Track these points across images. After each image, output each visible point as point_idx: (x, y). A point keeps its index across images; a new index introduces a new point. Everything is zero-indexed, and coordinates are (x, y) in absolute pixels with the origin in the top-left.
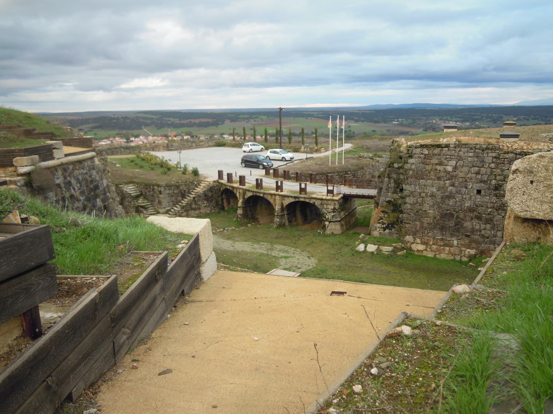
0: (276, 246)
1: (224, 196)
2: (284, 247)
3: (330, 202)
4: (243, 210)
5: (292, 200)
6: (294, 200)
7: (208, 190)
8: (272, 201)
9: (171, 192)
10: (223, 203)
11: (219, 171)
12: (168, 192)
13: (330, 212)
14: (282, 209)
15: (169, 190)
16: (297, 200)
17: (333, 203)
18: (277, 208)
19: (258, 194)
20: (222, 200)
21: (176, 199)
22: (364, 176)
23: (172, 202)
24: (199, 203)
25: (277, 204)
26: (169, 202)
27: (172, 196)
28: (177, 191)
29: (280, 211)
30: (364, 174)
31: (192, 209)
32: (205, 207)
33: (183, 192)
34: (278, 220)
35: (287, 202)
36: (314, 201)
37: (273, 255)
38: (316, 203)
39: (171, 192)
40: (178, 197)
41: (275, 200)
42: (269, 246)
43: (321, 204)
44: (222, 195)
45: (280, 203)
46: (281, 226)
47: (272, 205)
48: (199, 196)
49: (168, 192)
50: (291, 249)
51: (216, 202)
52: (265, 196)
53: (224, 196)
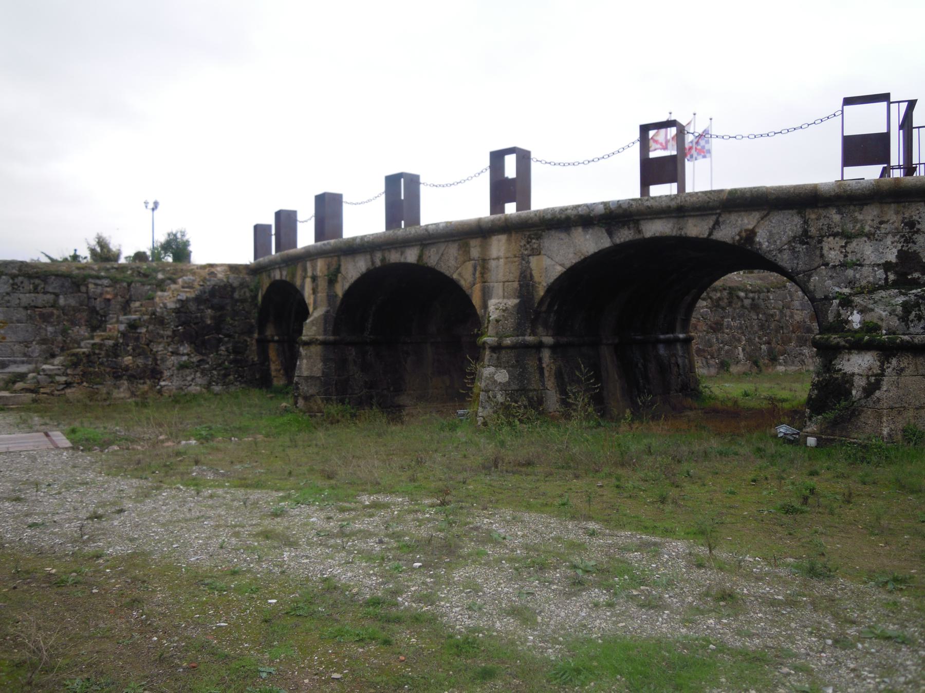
0: (492, 522)
1: (270, 331)
2: (573, 531)
3: (868, 216)
4: (325, 360)
5: (590, 243)
6: (605, 242)
7: (198, 300)
8: (464, 276)
10: (265, 358)
11: (257, 228)
12: (26, 299)
13: (874, 288)
14: (529, 310)
15: (36, 290)
16: (625, 235)
17: (893, 216)
18: (498, 305)
19: (394, 257)
20: (263, 343)
21: (64, 332)
22: (788, 312)
23: (44, 341)
24: (159, 348)
25: (498, 289)
27: (46, 318)
28: (72, 302)
29: (510, 323)
30: (787, 306)
31: (118, 374)
32: (183, 367)
33: (98, 304)
34: (502, 376)
35: (556, 259)
36: (748, 221)
37: (456, 614)
38: (762, 238)
40: (73, 323)
41: (483, 265)
42: (423, 521)
43: (804, 237)
44: (262, 327)
45: (514, 272)
46: (524, 403)
47: (466, 299)
48: (160, 321)
50: (653, 550)
51: (236, 351)
52: (432, 258)
53: (270, 331)
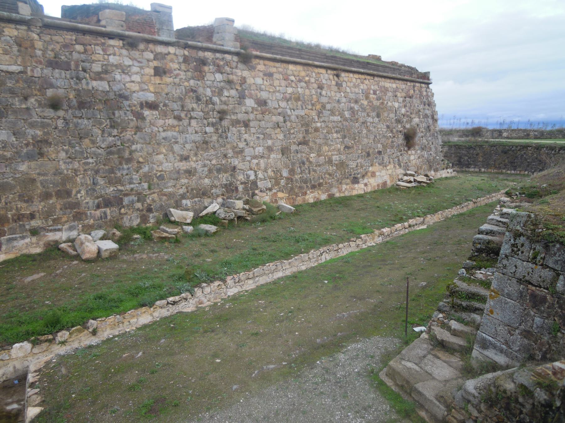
9: (542, 274)
12: (523, 267)
23: (527, 334)
26: (511, 329)
39: (542, 274)
49: (523, 267)
